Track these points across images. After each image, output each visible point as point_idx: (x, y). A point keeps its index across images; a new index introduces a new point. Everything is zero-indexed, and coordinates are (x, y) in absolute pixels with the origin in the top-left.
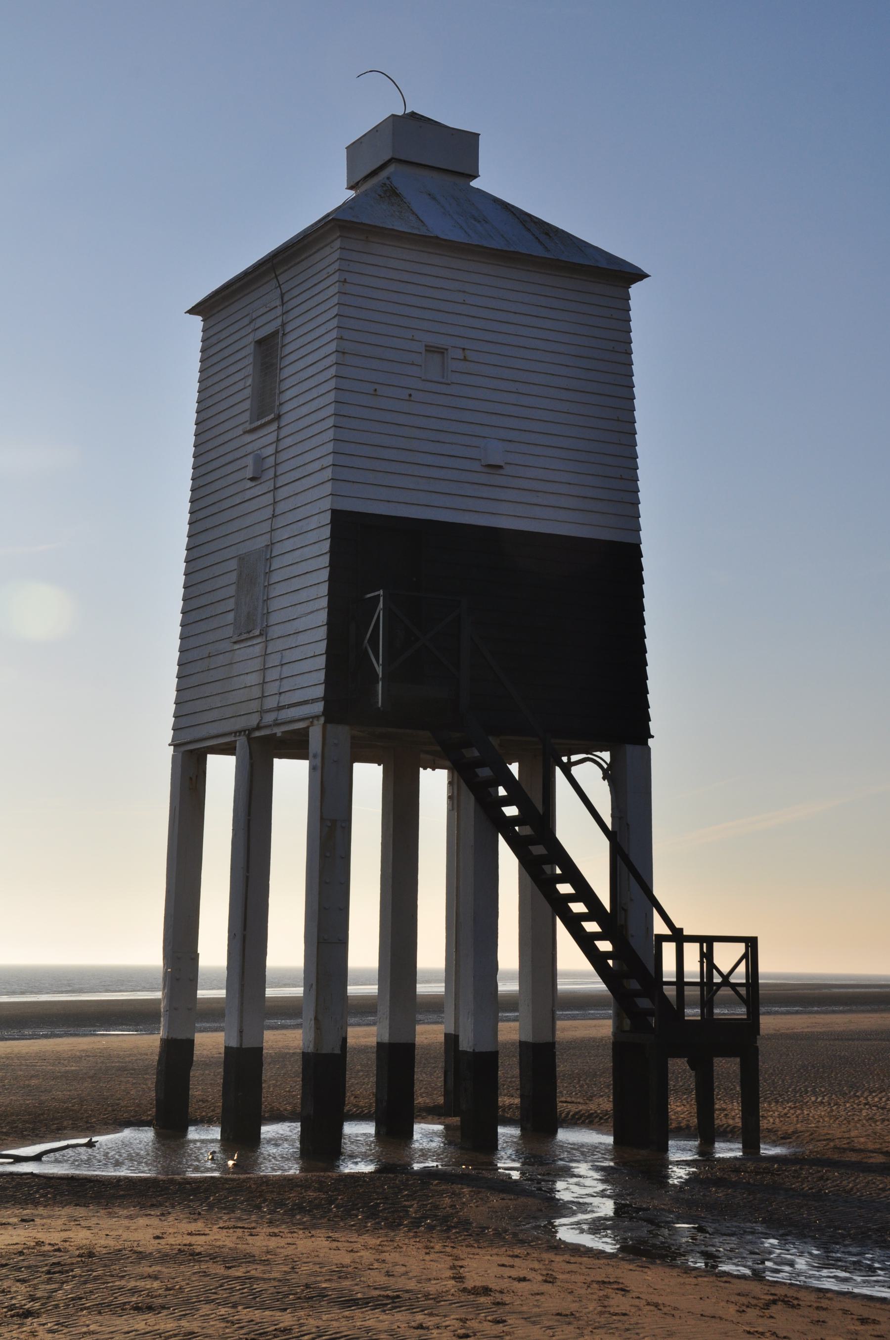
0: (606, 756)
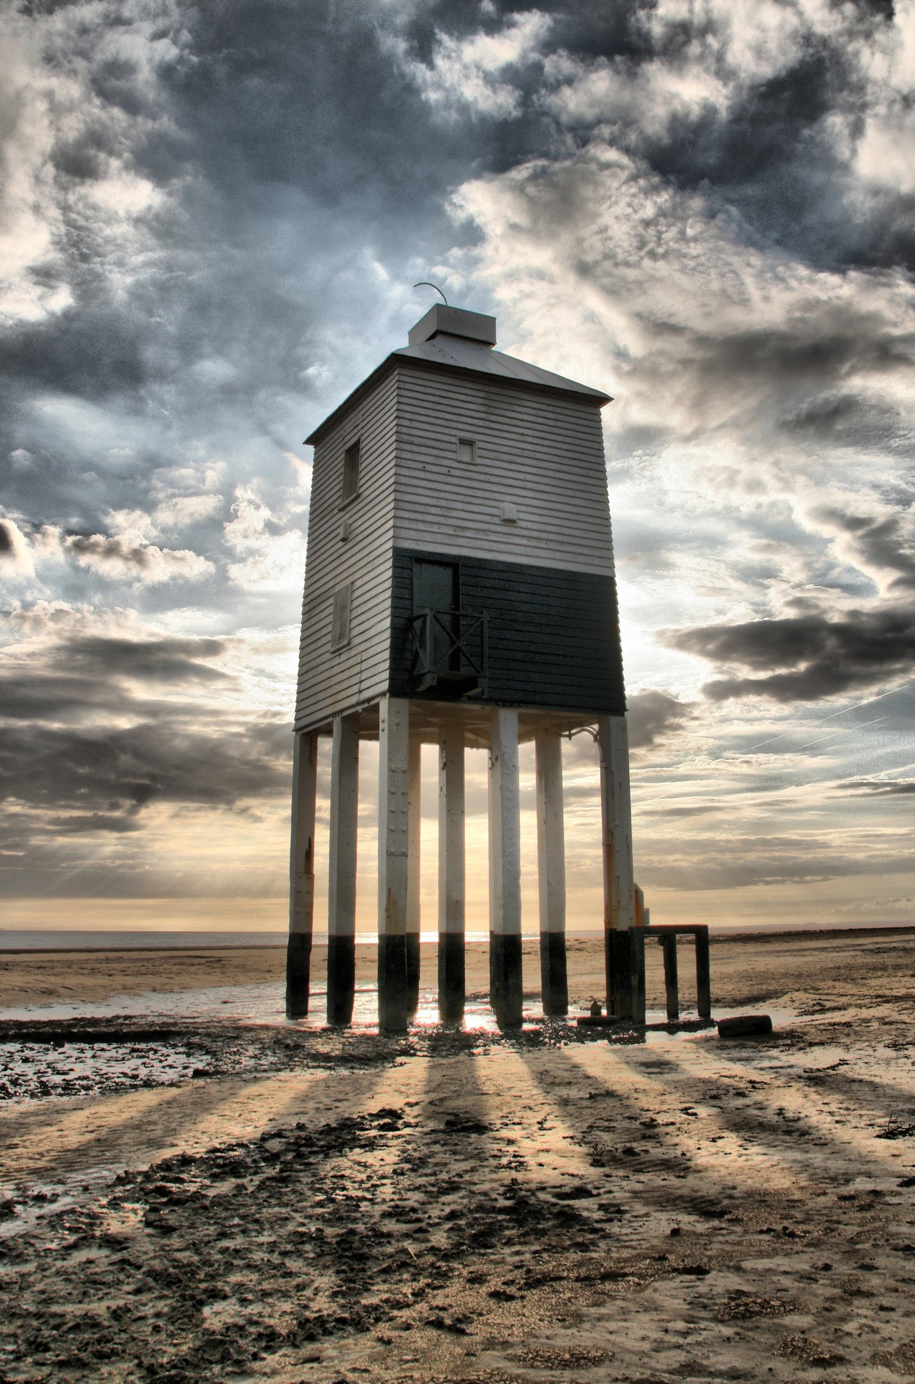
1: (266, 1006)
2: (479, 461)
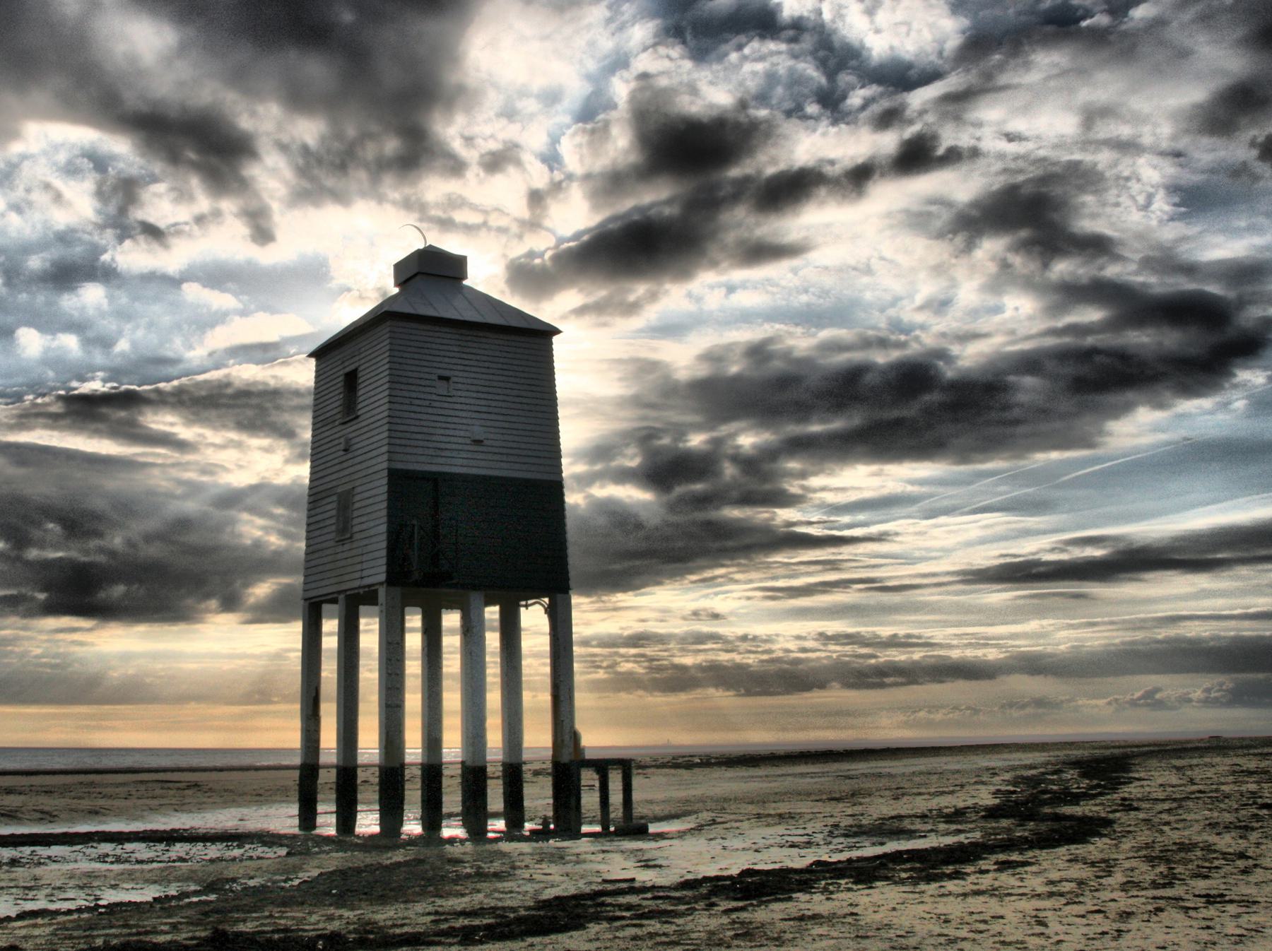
0: (546, 600)
1: (284, 818)
2: (455, 393)
